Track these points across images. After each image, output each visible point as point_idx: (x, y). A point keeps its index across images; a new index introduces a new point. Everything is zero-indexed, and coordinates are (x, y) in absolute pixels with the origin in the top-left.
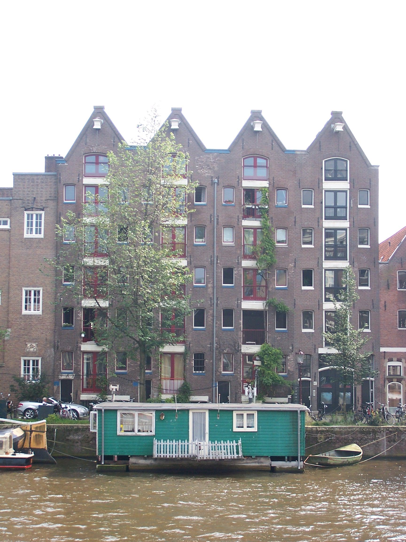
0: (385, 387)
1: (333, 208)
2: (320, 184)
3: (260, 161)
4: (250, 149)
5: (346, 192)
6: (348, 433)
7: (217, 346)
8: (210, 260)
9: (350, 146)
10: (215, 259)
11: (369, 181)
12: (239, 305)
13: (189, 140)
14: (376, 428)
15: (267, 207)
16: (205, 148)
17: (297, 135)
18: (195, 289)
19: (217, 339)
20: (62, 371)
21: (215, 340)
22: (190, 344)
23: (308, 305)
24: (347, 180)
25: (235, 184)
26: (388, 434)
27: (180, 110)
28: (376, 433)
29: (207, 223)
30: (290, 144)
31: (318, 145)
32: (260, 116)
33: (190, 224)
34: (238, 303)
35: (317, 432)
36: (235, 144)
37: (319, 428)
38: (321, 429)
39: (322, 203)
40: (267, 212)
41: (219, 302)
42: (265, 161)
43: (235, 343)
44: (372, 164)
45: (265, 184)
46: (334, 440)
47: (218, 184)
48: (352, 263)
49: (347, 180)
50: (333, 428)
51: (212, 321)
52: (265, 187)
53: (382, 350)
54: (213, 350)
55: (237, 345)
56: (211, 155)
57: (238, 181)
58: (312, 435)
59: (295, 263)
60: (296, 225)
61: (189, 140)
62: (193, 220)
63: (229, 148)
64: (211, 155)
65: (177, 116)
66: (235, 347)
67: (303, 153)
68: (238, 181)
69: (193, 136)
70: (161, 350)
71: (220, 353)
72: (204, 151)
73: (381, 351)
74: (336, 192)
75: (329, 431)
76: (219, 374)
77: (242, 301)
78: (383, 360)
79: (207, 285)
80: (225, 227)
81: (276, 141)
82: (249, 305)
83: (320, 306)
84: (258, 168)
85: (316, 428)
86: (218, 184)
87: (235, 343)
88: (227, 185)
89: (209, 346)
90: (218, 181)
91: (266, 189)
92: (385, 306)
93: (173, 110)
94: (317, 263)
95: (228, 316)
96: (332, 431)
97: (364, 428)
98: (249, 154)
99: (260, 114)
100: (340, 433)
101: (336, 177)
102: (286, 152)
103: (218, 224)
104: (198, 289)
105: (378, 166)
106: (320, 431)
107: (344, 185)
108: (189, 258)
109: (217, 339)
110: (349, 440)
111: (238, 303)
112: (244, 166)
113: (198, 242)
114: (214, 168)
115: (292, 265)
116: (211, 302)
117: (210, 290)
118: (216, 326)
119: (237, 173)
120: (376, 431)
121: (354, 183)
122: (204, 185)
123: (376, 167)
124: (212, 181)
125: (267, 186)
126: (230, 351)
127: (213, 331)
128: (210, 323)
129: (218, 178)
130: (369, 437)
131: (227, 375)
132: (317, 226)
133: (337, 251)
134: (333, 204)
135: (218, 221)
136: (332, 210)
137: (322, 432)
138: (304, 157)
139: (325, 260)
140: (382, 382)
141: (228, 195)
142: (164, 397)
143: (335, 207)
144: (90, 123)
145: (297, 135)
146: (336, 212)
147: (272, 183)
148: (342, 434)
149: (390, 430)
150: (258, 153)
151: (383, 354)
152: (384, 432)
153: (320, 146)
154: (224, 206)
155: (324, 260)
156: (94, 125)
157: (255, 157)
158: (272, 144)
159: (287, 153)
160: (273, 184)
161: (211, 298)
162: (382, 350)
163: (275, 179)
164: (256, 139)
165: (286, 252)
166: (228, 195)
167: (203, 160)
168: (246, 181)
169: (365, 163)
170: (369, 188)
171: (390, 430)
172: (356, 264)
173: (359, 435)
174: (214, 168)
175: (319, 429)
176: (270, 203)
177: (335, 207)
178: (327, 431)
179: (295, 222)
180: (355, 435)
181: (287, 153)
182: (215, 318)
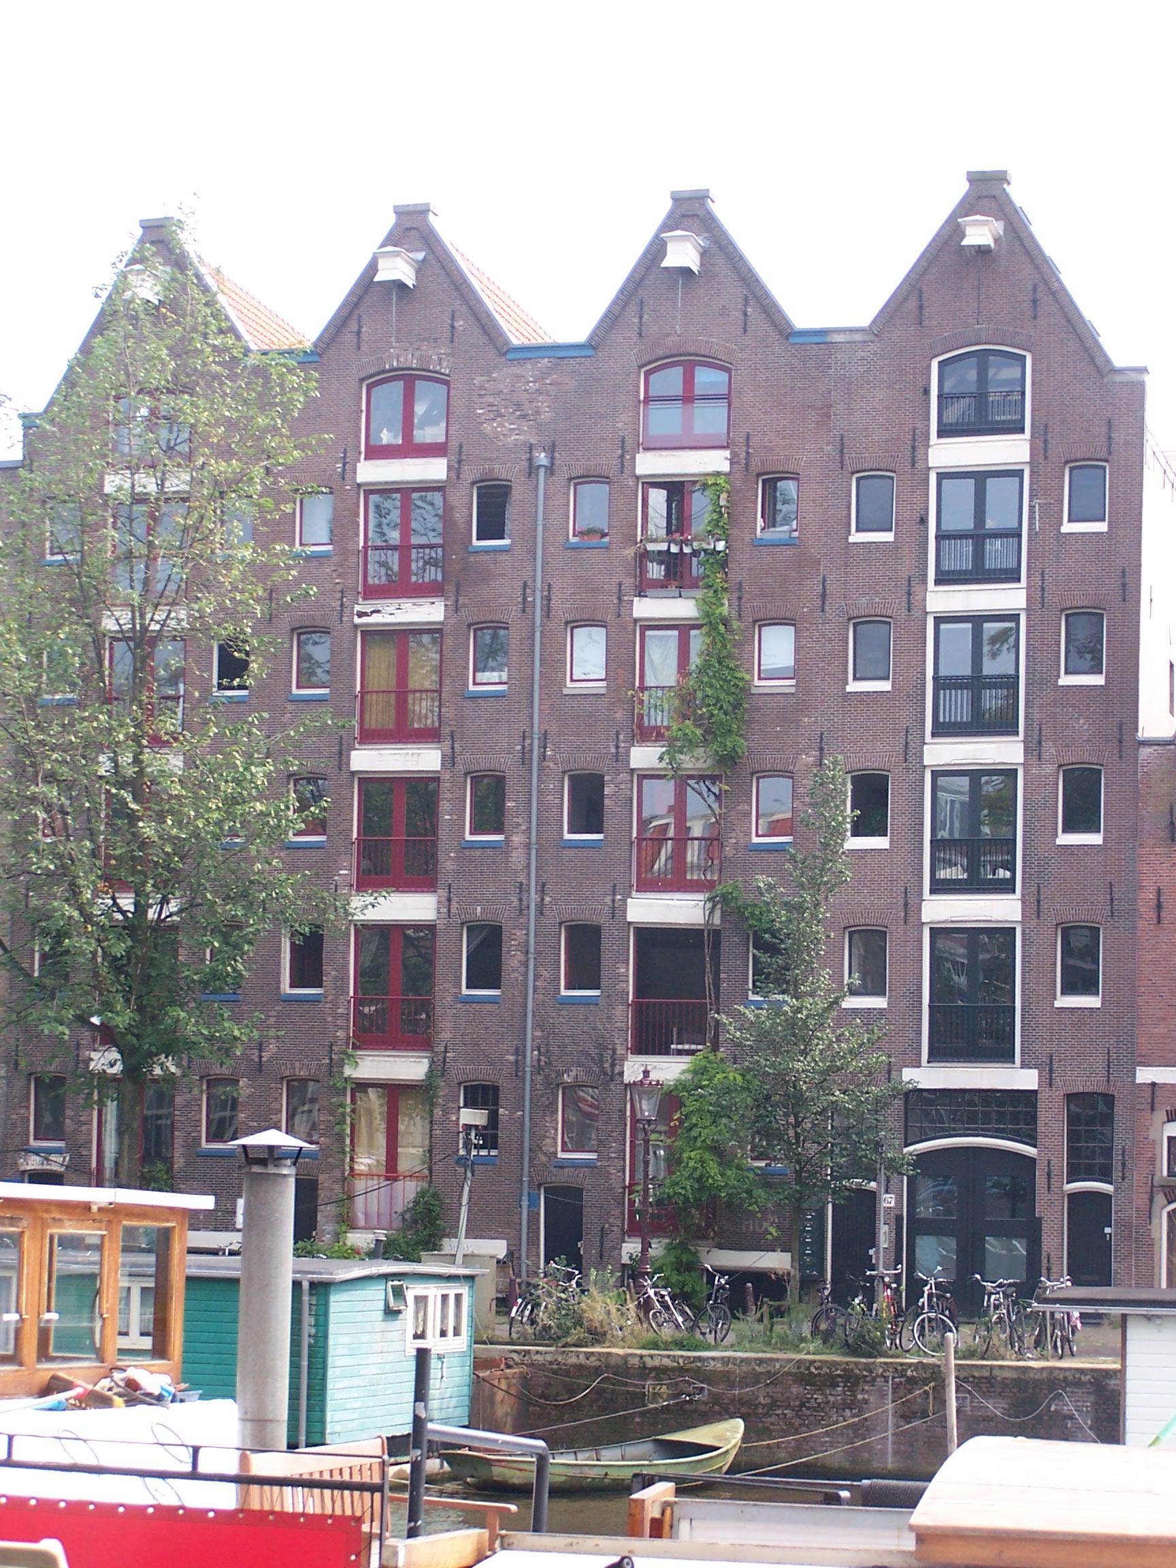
0: (1155, 1221)
1: (971, 537)
2: (920, 451)
3: (706, 379)
4: (668, 335)
5: (1019, 474)
6: (756, 1378)
7: (539, 1060)
8: (519, 748)
9: (1034, 301)
10: (536, 742)
11: (1105, 429)
12: (618, 911)
13: (453, 319)
14: (856, 1364)
15: (721, 546)
16: (788, 324)
17: (836, 271)
18: (467, 852)
19: (538, 1034)
20: (33, 1143)
21: (529, 1037)
22: (446, 1052)
23: (871, 906)
24: (1022, 431)
25: (613, 471)
26: (902, 1391)
27: (422, 212)
28: (856, 1384)
29: (512, 615)
30: (806, 309)
31: (912, 304)
32: (701, 213)
33: (452, 621)
34: (613, 901)
35: (644, 1371)
36: (611, 320)
37: (651, 1356)
38: (657, 1362)
39: (923, 521)
40: (724, 564)
41: (547, 899)
42: (724, 377)
43: (602, 1047)
44: (1118, 361)
45: (717, 461)
46: (706, 1404)
47: (550, 470)
48: (1033, 748)
49: (1022, 431)
50: (700, 1359)
51: (522, 969)
52: (718, 474)
53: (1145, 1075)
54: (524, 1072)
55: (608, 1054)
56: (529, 366)
57: (622, 456)
58: (626, 1384)
59: (821, 749)
60: (827, 608)
61: (453, 319)
62: (464, 605)
63: (591, 338)
64: (529, 366)
65: (413, 233)
66: (601, 1061)
67: (858, 337)
68: (622, 456)
69: (466, 302)
70: (348, 1071)
71: (547, 1082)
72: (505, 354)
73: (1138, 1081)
74: (980, 478)
75: (687, 1370)
76: (544, 1159)
77: (634, 894)
78: (1147, 1114)
79: (507, 841)
80: (575, 623)
81: (757, 299)
82: (646, 909)
83: (910, 909)
84: (697, 404)
85: (641, 1357)
86: (550, 470)
87: (602, 1047)
88: (580, 473)
89: (512, 1058)
90: (553, 458)
91: (721, 481)
92: (1159, 906)
93: (679, 199)
94: (901, 748)
95: (586, 949)
96: (696, 1371)
97: (812, 1362)
98: (660, 353)
99: (703, 205)
100: (726, 1378)
101: (980, 419)
102: (793, 340)
103: (547, 613)
104: (478, 853)
105: (1144, 370)
106: (654, 1368)
107: (1010, 450)
108: (448, 743)
109: (538, 1034)
110: (756, 1406)
111: (613, 901)
112: (647, 400)
113: (492, 680)
114: (538, 413)
115: (808, 759)
116: (521, 900)
117: (517, 857)
118: (535, 988)
119: (620, 425)
120: (857, 1377)
121: (1046, 441)
122: (503, 477)
123: (1133, 376)
124: (530, 460)
125: (725, 467)
126: (583, 1077)
127: (525, 1006)
128: (516, 975)
129: (552, 449)
130: (832, 1399)
131: (574, 1164)
132: (904, 612)
133: (982, 705)
134: (990, 524)
135: (548, 606)
136: (968, 547)
137: (660, 1373)
138: (860, 354)
139: (933, 735)
140: (1140, 1200)
141: (591, 506)
142: (360, 1239)
143: (979, 536)
144: (952, 231)
145: (836, 271)
146: (979, 554)
147: (743, 455)
148: (732, 1385)
149: (909, 1373)
150: (692, 350)
151: (1147, 1093)
152: (886, 1379)
153: (921, 307)
154: (574, 548)
155: (928, 737)
156: (963, 236)
157: (689, 363)
158: (745, 314)
159: (800, 340)
160: (747, 459)
161: (521, 884)
162: (1145, 1075)
163: (754, 441)
164: (413, 314)
165: (790, 710)
166: (591, 506)
167: (501, 387)
168: (650, 455)
169: (1092, 360)
170: (1104, 455)
171: (909, 1373)
172: (1049, 749)
173: (795, 1390)
174: (538, 413)
175: (650, 1363)
176: (734, 532)
177: (979, 536)
178: (681, 1370)
179: (824, 595)
180: (778, 1389)
181: (800, 340)
182: (531, 956)
